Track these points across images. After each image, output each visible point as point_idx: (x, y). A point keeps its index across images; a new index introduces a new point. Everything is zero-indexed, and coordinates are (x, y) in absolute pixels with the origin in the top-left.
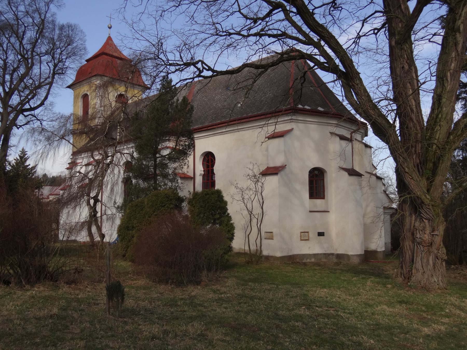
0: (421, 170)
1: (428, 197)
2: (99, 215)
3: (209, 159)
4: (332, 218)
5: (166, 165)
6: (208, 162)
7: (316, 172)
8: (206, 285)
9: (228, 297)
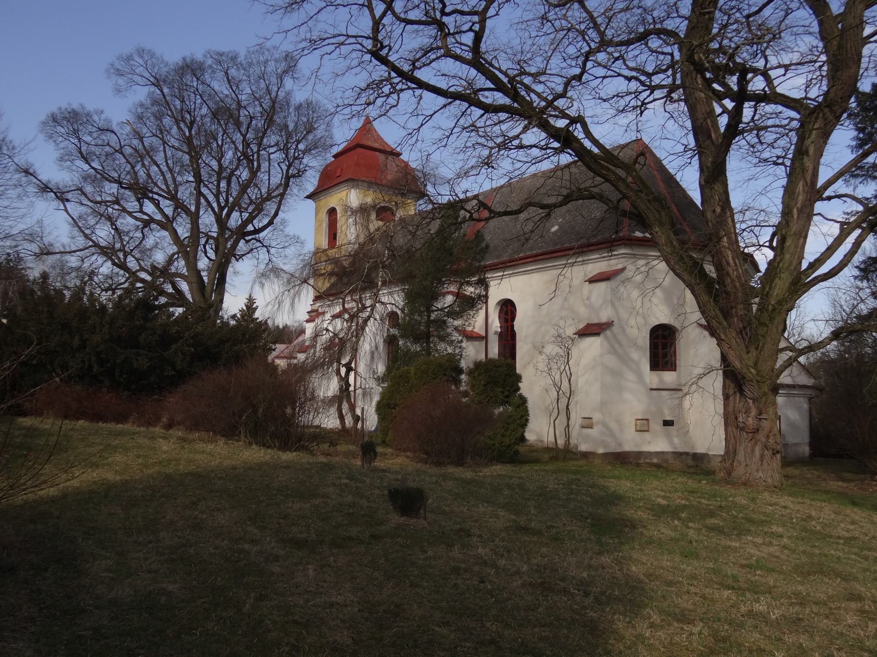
1: (753, 371)
2: (352, 388)
3: (508, 309)
5: (445, 322)
6: (506, 314)
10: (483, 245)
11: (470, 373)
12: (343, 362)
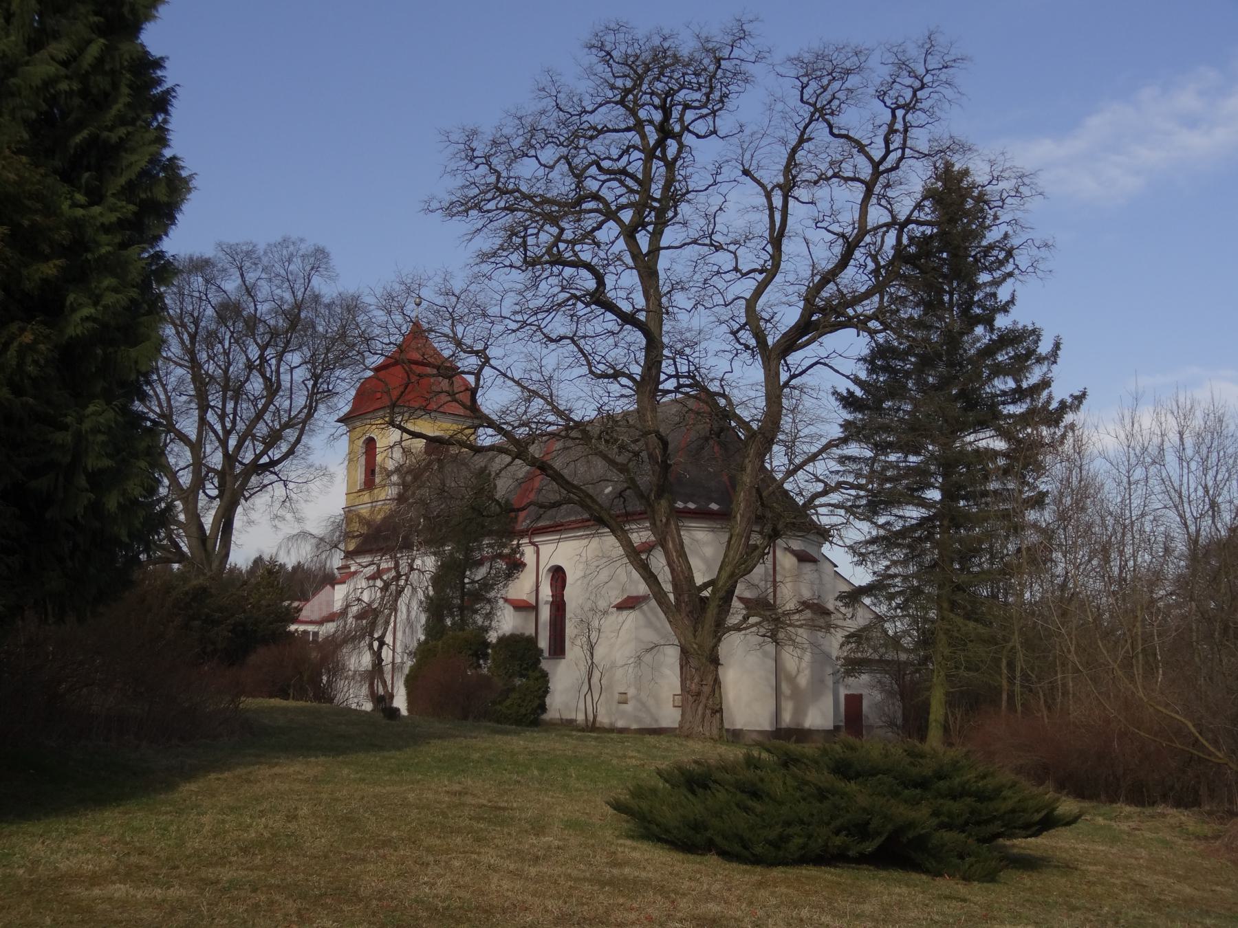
3: (558, 575)
12: (376, 636)
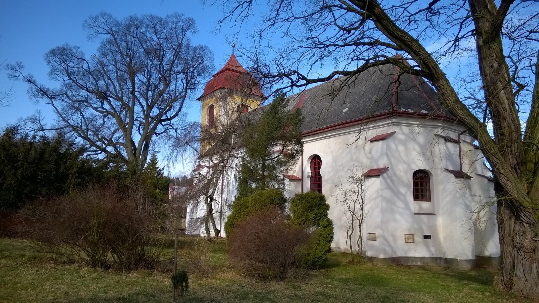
0: (519, 171)
1: (528, 199)
3: (316, 161)
4: (440, 221)
6: (315, 164)
7: (421, 174)
8: (290, 282)
9: (304, 294)
10: (301, 117)
11: (293, 202)
